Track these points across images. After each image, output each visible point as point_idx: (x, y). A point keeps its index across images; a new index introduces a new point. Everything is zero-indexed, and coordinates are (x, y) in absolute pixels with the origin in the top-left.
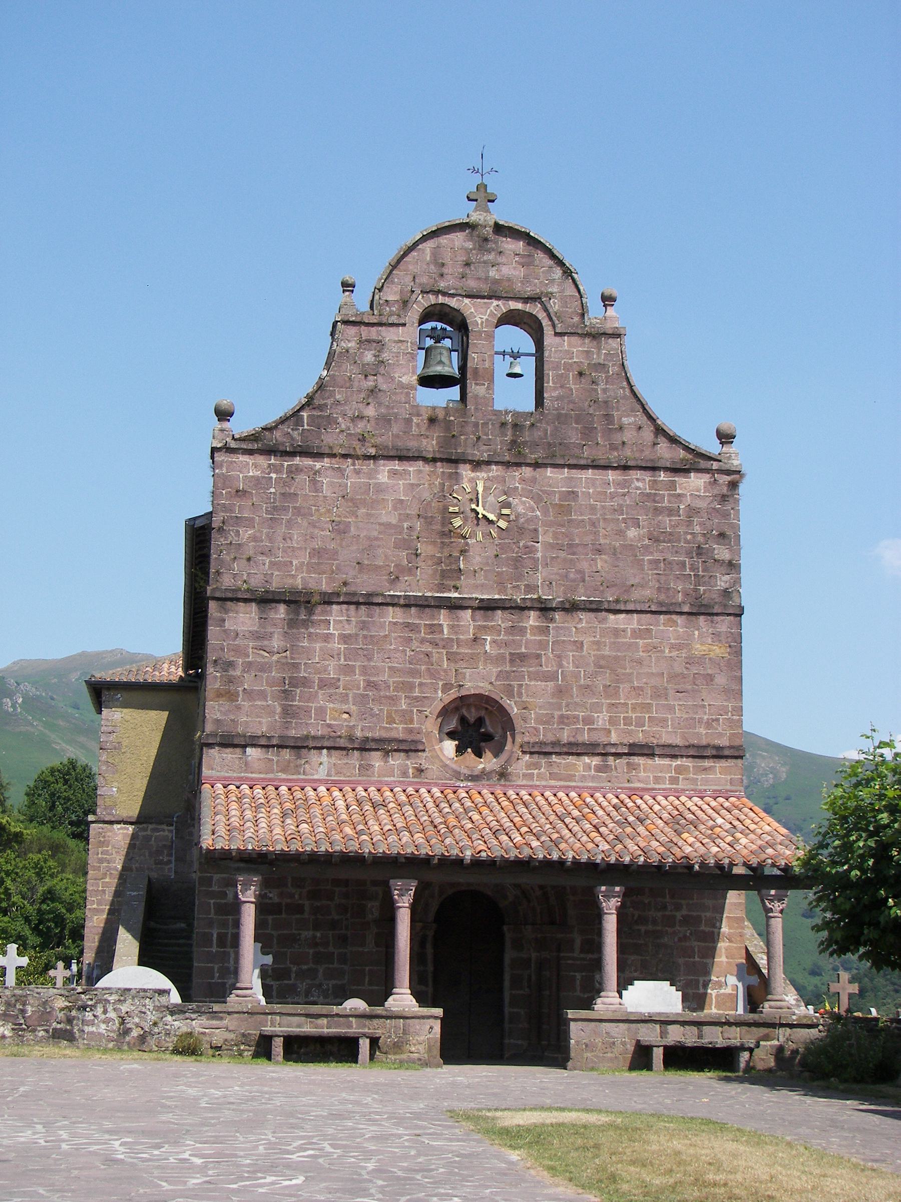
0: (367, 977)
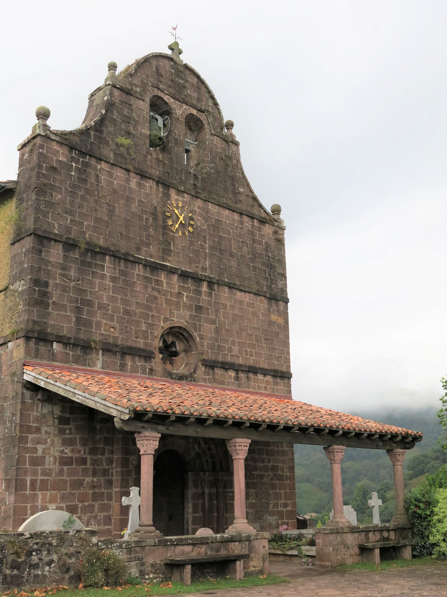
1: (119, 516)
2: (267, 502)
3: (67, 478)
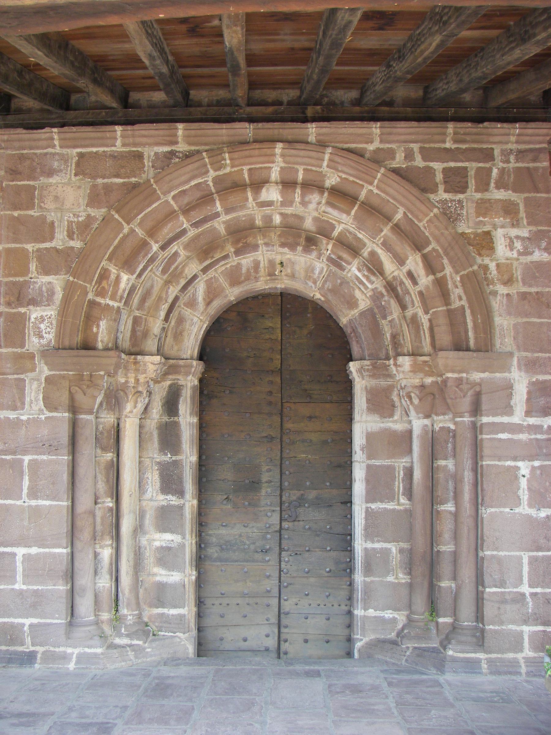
0: (26, 479)
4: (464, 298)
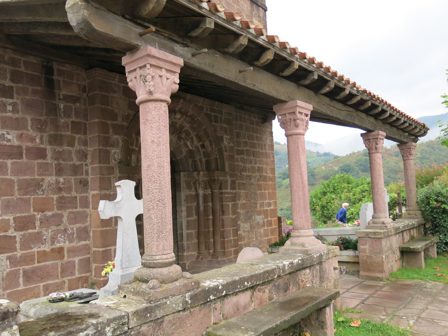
1: (99, 227)
2: (255, 202)
3: (13, 178)
4: (218, 155)
